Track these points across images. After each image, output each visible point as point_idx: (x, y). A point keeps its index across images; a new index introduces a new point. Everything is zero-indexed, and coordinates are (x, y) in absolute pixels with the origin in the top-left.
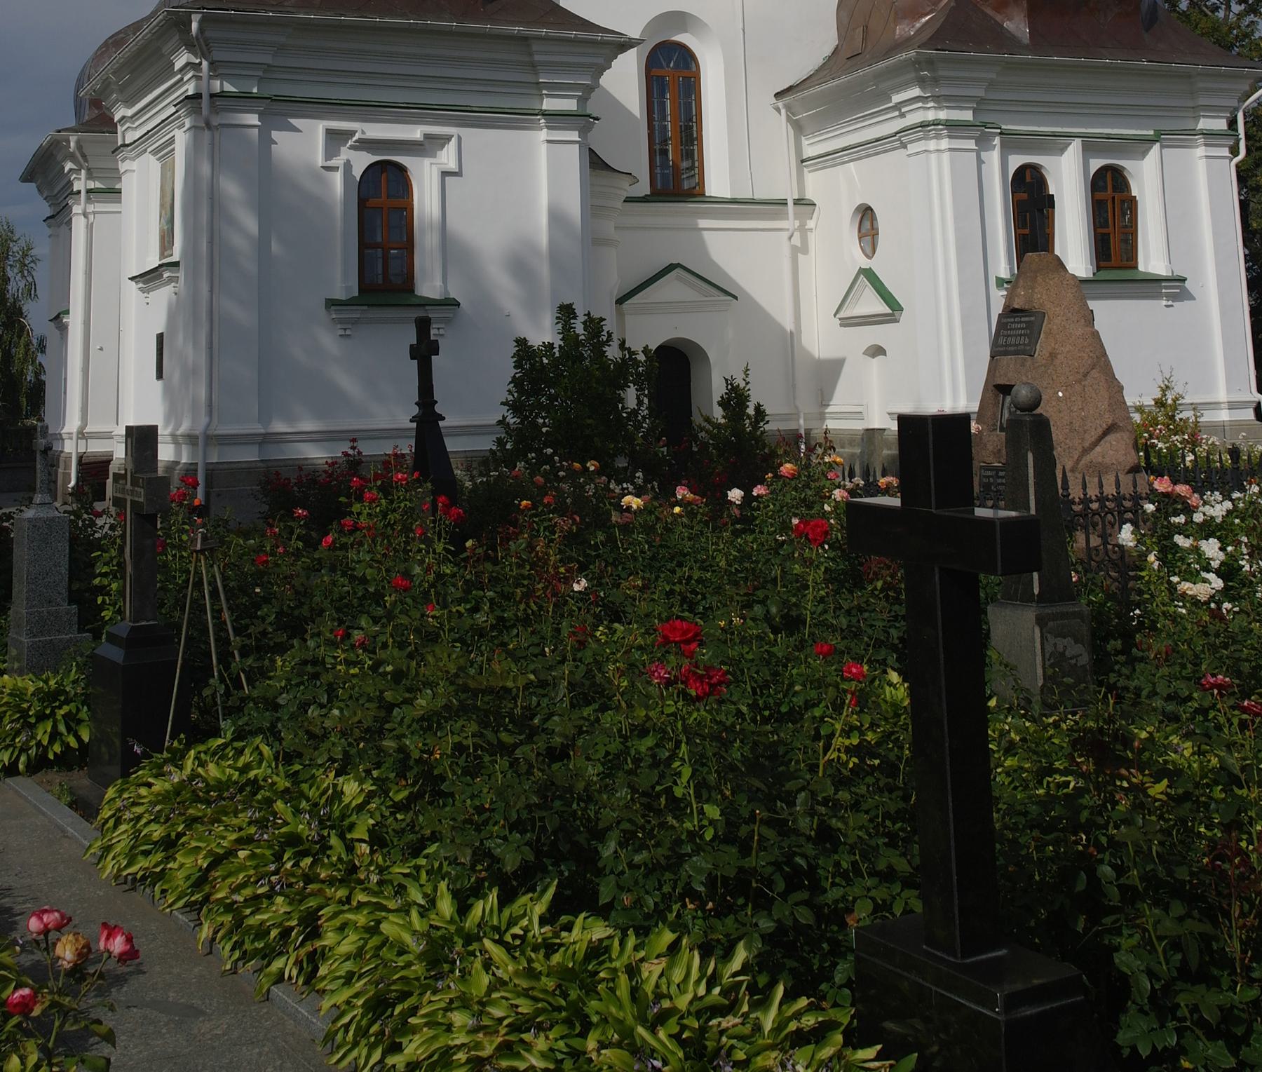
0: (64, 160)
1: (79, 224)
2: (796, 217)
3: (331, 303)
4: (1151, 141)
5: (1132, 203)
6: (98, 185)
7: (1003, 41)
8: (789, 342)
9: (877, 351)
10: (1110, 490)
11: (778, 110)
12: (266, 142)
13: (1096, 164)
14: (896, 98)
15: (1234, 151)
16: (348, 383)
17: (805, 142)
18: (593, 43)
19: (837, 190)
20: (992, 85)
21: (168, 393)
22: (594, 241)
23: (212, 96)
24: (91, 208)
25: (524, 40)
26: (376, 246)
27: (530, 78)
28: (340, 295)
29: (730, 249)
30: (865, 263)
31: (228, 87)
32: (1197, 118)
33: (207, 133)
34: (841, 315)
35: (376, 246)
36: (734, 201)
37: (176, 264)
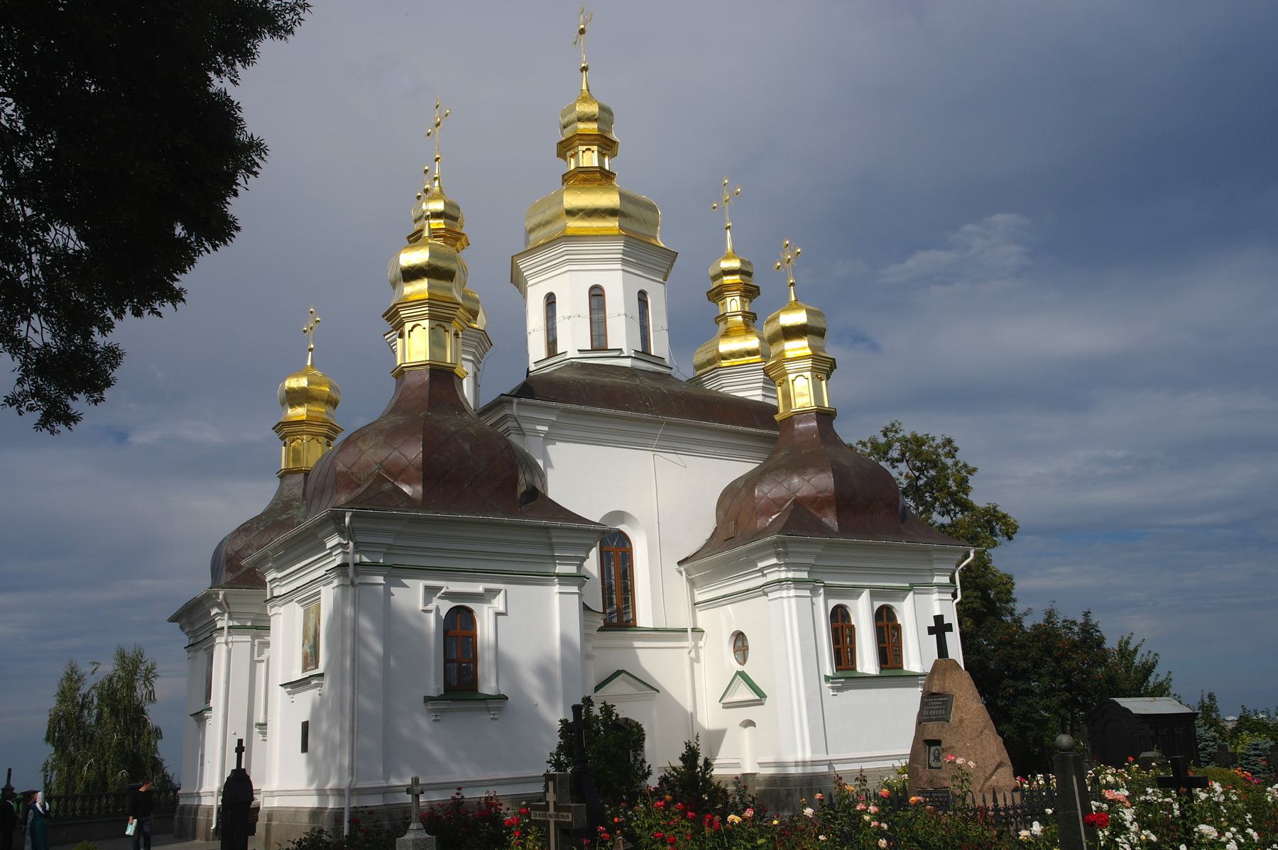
0: (212, 607)
1: (220, 653)
2: (693, 639)
3: (428, 699)
4: (907, 590)
5: (898, 628)
6: (236, 623)
7: (823, 530)
8: (691, 718)
9: (749, 723)
10: (1009, 802)
11: (680, 572)
12: (388, 594)
13: (877, 604)
14: (760, 565)
15: (954, 596)
16: (436, 751)
17: (696, 592)
18: (589, 530)
19: (719, 624)
20: (818, 557)
21: (312, 762)
22: (586, 656)
23: (355, 565)
24: (230, 639)
25: (546, 528)
26: (453, 661)
27: (548, 553)
28: (433, 693)
29: (654, 660)
30: (740, 668)
31: (365, 559)
32: (933, 576)
33: (350, 590)
34: (724, 701)
35: (453, 661)
36: (655, 630)
37: (322, 675)
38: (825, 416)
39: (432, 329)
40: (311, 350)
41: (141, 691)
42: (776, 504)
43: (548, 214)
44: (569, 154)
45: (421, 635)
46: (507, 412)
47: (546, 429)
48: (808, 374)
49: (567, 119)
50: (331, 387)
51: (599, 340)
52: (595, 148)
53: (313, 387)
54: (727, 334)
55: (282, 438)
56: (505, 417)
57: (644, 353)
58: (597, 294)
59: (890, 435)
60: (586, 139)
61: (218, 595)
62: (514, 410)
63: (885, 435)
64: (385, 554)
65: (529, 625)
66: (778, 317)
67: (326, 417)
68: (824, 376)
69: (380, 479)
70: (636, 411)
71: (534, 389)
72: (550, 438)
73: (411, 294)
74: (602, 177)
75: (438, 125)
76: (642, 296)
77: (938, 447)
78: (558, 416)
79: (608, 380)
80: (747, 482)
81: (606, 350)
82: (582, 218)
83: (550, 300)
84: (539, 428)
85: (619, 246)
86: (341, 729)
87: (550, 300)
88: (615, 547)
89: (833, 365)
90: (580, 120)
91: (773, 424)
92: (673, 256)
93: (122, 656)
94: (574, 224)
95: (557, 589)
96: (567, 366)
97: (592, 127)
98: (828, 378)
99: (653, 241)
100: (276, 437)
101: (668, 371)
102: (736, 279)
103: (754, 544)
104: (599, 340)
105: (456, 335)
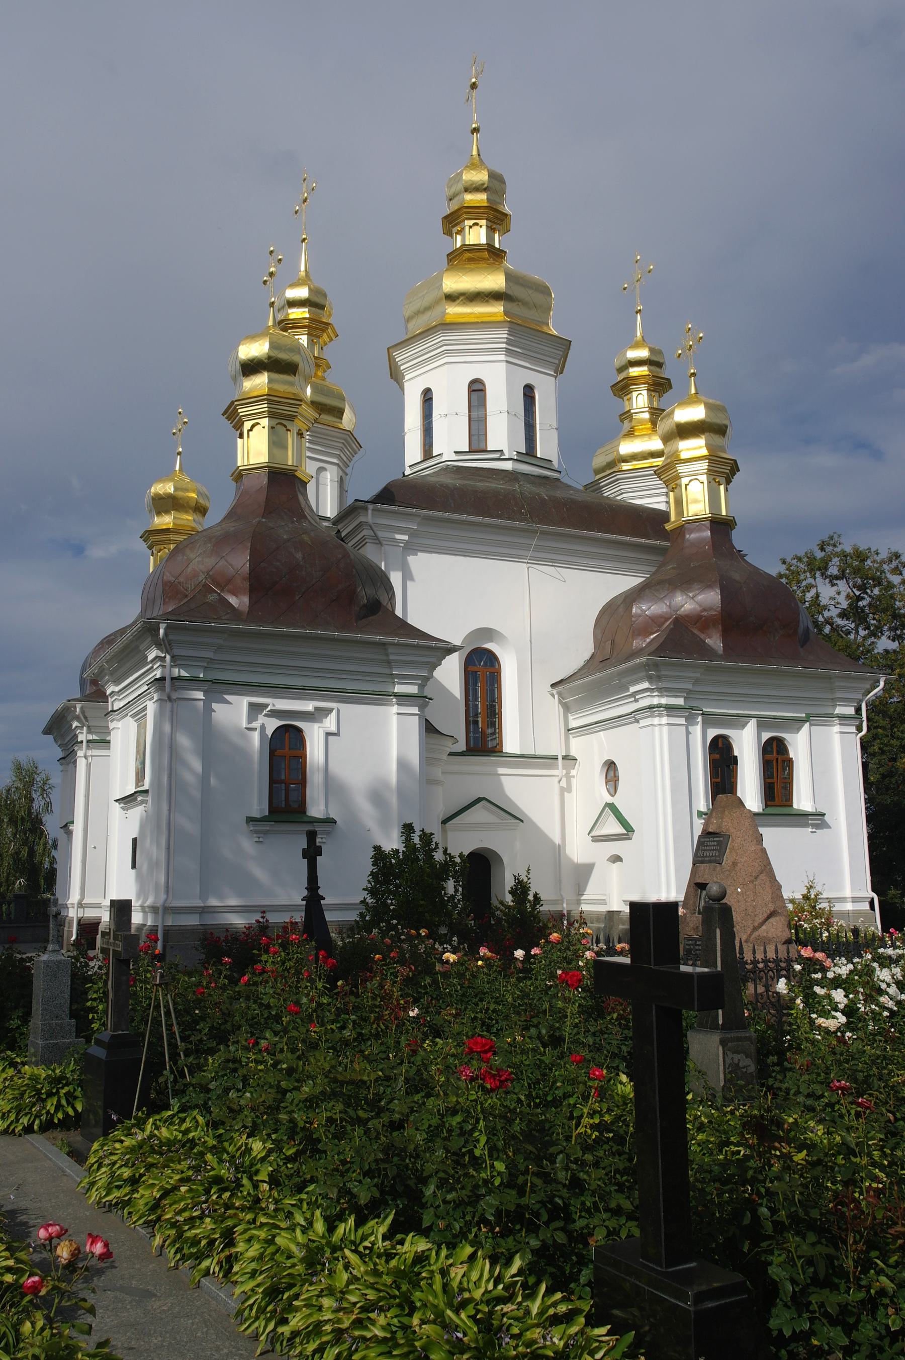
0: (72, 720)
1: (81, 764)
2: (564, 767)
3: (250, 820)
4: (803, 721)
5: (789, 763)
6: (95, 737)
7: (705, 652)
8: (557, 852)
9: (617, 859)
11: (553, 695)
12: (209, 710)
13: (766, 736)
14: (633, 689)
15: (859, 729)
16: (260, 873)
17: (571, 717)
18: (430, 648)
19: (592, 750)
20: (697, 681)
21: (140, 878)
22: (427, 781)
23: (173, 679)
24: (89, 753)
25: (383, 645)
26: (281, 782)
29: (519, 788)
30: (609, 799)
31: (184, 673)
32: (834, 706)
33: (169, 704)
34: (593, 834)
37: (146, 791)
38: (721, 526)
39: (272, 428)
40: (179, 453)
41: (38, 803)
42: (655, 622)
43: (426, 302)
44: (454, 230)
45: (243, 753)
46: (362, 519)
47: (406, 538)
48: (704, 478)
49: (453, 190)
50: (199, 493)
52: (483, 222)
53: (180, 494)
54: (630, 434)
55: (150, 548)
56: (360, 524)
58: (477, 389)
59: (829, 549)
60: (473, 212)
61: (75, 708)
62: (369, 517)
63: (822, 549)
64: (206, 668)
65: (366, 749)
66: (672, 412)
67: (194, 525)
68: (723, 480)
69: (207, 590)
70: (509, 519)
71: (400, 495)
72: (410, 548)
73: (251, 390)
74: (491, 255)
75: (305, 201)
76: (529, 392)
77: (883, 562)
78: (418, 525)
79: (481, 485)
80: (626, 597)
81: (485, 451)
82: (464, 304)
83: (427, 397)
84: (398, 537)
85: (503, 334)
86: (158, 845)
87: (427, 397)
88: (482, 668)
89: (734, 468)
90: (467, 190)
91: (664, 535)
92: (565, 345)
93: (19, 768)
94: (454, 311)
95: (837, 728)
96: (442, 469)
97: (480, 198)
98: (728, 482)
99: (545, 329)
100: (143, 546)
101: (556, 475)
102: (643, 370)
103: (624, 666)
105: (300, 434)
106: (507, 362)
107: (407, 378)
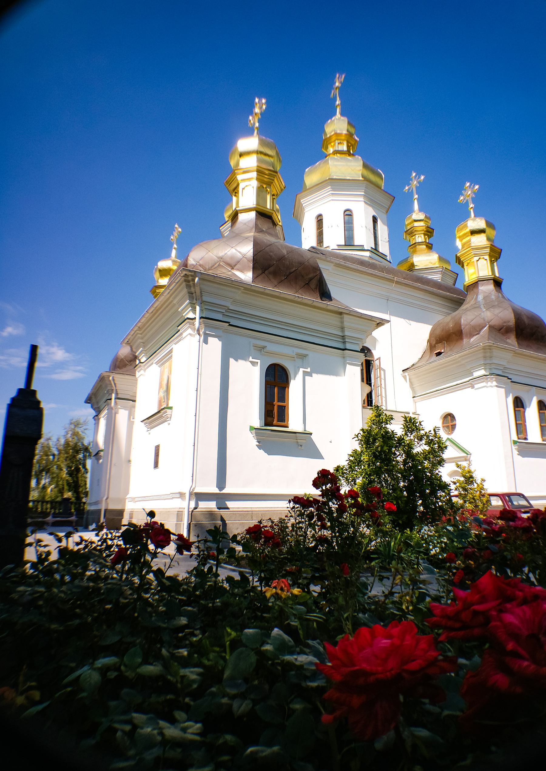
11: (405, 377)
48: (487, 257)
51: (349, 241)
57: (375, 250)
58: (348, 214)
83: (320, 221)
87: (320, 221)
104: (349, 241)
106: (365, 202)
107: (306, 210)
